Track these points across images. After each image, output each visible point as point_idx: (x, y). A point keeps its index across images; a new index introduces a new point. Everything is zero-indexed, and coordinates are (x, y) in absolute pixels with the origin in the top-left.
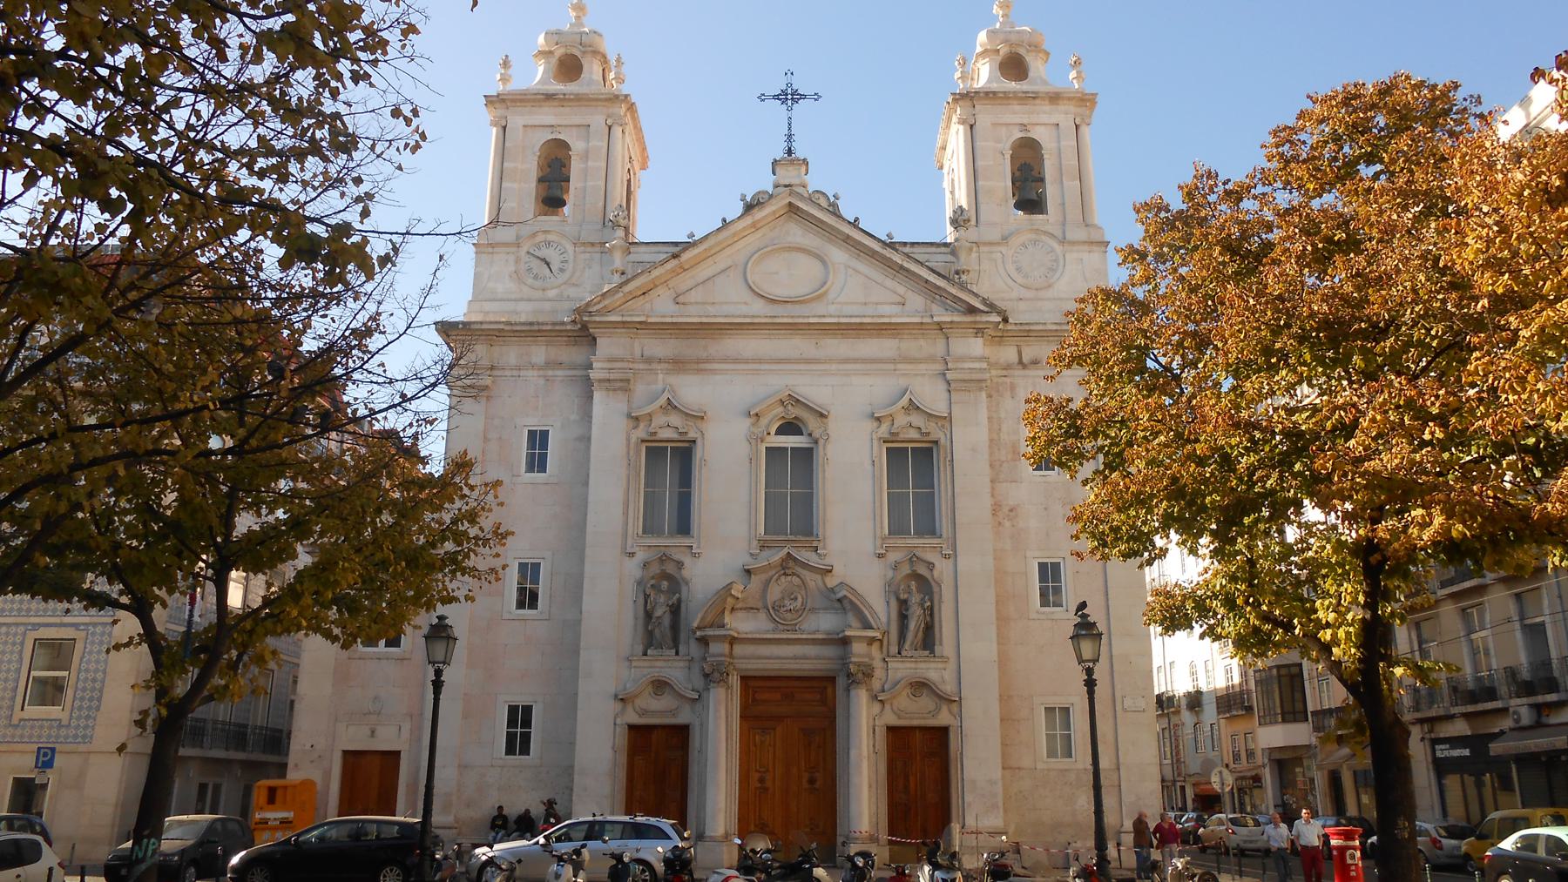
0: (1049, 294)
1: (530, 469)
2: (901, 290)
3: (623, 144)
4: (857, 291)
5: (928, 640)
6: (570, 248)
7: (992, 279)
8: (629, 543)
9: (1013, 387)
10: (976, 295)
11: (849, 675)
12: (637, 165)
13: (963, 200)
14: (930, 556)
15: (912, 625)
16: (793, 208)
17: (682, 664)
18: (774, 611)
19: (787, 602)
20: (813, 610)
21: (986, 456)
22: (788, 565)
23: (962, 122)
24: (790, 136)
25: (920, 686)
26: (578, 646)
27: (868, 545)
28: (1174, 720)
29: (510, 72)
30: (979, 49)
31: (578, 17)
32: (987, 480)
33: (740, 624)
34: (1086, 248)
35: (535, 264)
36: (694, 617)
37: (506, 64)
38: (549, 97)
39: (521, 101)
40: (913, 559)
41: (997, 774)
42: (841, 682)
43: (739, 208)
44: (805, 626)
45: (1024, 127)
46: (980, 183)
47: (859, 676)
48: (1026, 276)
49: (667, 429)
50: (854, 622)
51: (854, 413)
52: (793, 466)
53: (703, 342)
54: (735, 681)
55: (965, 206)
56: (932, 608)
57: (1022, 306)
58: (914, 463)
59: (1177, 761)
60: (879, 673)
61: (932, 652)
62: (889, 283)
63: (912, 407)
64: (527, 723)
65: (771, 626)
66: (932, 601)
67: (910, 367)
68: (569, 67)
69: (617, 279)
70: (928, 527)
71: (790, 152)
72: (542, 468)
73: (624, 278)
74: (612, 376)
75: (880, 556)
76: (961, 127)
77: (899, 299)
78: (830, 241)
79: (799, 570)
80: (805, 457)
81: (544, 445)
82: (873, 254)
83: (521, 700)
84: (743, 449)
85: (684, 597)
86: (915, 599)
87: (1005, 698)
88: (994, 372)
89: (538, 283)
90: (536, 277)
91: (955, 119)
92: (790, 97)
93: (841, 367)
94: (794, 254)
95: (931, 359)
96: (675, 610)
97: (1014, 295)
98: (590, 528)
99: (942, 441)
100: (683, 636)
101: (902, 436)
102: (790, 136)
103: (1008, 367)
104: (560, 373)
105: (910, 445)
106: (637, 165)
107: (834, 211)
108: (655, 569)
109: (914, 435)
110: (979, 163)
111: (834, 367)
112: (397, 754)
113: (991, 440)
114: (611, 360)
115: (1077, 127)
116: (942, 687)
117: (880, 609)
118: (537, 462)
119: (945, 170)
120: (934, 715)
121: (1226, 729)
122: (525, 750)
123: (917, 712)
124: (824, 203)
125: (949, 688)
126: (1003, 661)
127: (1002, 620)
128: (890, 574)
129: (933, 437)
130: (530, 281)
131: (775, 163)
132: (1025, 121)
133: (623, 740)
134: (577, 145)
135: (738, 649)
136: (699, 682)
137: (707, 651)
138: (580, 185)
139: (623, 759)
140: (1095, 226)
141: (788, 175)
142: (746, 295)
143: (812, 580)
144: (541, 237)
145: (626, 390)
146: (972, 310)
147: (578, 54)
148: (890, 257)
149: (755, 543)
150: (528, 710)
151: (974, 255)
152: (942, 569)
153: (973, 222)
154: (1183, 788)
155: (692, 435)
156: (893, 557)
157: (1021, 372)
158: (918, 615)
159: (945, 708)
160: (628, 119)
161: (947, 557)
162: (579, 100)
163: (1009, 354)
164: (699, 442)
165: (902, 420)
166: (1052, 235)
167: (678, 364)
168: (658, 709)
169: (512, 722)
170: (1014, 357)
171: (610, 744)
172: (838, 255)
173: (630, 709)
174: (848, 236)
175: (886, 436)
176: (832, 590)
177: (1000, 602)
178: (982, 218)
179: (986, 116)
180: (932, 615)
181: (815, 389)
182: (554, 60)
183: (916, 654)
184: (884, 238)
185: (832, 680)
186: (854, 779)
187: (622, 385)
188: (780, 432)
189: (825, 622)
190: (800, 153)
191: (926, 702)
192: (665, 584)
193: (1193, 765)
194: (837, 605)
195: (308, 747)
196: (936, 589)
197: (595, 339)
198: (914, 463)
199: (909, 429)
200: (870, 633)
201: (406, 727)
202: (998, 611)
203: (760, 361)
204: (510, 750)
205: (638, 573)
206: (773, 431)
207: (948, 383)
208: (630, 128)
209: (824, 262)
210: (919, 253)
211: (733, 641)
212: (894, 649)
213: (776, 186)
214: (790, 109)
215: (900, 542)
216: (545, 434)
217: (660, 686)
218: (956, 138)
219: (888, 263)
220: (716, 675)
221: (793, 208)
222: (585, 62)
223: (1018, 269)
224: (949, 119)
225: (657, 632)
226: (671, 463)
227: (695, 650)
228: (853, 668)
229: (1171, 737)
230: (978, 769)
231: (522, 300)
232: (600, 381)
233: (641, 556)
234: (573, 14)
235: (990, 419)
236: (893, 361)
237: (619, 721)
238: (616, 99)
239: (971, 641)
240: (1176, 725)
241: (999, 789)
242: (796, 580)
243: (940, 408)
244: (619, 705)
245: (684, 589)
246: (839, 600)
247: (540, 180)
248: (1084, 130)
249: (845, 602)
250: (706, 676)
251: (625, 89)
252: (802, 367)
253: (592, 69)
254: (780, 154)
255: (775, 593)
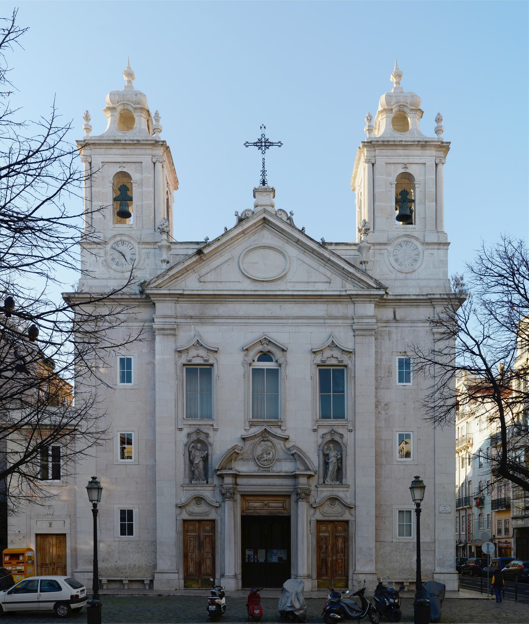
0: (414, 275)
1: (123, 381)
2: (329, 274)
3: (163, 174)
4: (304, 275)
5: (339, 474)
6: (136, 246)
7: (382, 268)
8: (180, 422)
9: (390, 333)
10: (371, 278)
11: (298, 494)
12: (171, 188)
13: (365, 216)
14: (341, 431)
15: (331, 468)
16: (265, 222)
17: (210, 488)
18: (257, 460)
19: (265, 455)
20: (279, 460)
21: (373, 374)
22: (265, 435)
23: (367, 161)
24: (264, 172)
25: (334, 500)
26: (155, 478)
27: (309, 425)
28: (469, 512)
29: (90, 123)
30: (380, 108)
31: (129, 82)
32: (374, 387)
33: (242, 467)
34: (436, 247)
35: (117, 255)
36: (215, 461)
37: (87, 118)
38: (116, 143)
39: (99, 144)
40: (333, 432)
41: (373, 544)
42: (293, 497)
43: (234, 221)
44: (274, 469)
45: (405, 166)
46: (376, 204)
47: (303, 495)
48: (400, 265)
49: (197, 357)
50: (302, 468)
51: (302, 343)
52: (266, 365)
53: (216, 306)
54: (238, 497)
55: (367, 220)
56: (341, 459)
57: (398, 283)
58: (332, 380)
59: (468, 532)
60: (313, 493)
61: (341, 482)
62: (322, 269)
63: (333, 346)
64: (131, 519)
65: (256, 468)
66: (341, 455)
67: (333, 321)
68: (126, 120)
69: (165, 266)
70: (340, 415)
71: (264, 183)
72: (129, 381)
73: (169, 266)
74: (166, 327)
75: (315, 430)
76: (366, 165)
77: (326, 280)
78: (288, 242)
79: (271, 438)
80: (274, 373)
81: (129, 367)
82: (313, 251)
83: (126, 507)
84: (240, 370)
85: (210, 453)
86: (333, 454)
87: (378, 506)
88: (379, 325)
89: (119, 268)
90: (117, 264)
91: (363, 159)
92: (263, 144)
93: (294, 321)
94: (267, 251)
95: (345, 318)
96: (205, 459)
97: (393, 276)
98: (157, 415)
99: (350, 366)
100: (210, 473)
101: (328, 363)
102: (264, 172)
103: (387, 322)
104: (135, 324)
105: (332, 368)
106: (171, 188)
107: (291, 225)
108: (194, 437)
109: (334, 362)
110: (376, 190)
111: (290, 321)
112: (65, 535)
113: (376, 365)
114: (164, 317)
115: (436, 164)
116: (346, 500)
117: (315, 460)
118: (126, 377)
119: (356, 192)
120: (342, 516)
121: (496, 518)
122: (131, 533)
123: (333, 512)
124: (285, 218)
125: (349, 501)
126: (378, 487)
127: (378, 465)
128: (320, 441)
129: (345, 363)
130: (114, 267)
131: (255, 191)
132: (406, 161)
133: (180, 528)
134: (135, 176)
135: (239, 481)
136: (219, 498)
137: (223, 482)
138: (139, 203)
139: (181, 538)
140: (443, 232)
141: (264, 199)
142: (240, 277)
143: (279, 444)
144: (118, 238)
145: (174, 335)
146: (369, 287)
147: (131, 109)
148: (321, 252)
149: (247, 423)
150: (130, 512)
151: (371, 251)
152: (348, 438)
153: (372, 230)
154: (470, 547)
155: (211, 362)
156: (322, 431)
157: (394, 325)
158: (334, 463)
159: (347, 511)
160: (165, 158)
161: (350, 431)
162: (137, 143)
163: (388, 313)
164: (215, 366)
165: (328, 353)
166: (417, 239)
167: (202, 319)
168: (198, 511)
169: (122, 519)
170: (391, 316)
171: (175, 530)
172: (292, 251)
173: (184, 512)
174: (298, 240)
175: (319, 363)
176: (289, 449)
177: (377, 455)
178: (377, 227)
179: (383, 156)
180: (341, 463)
181: (279, 335)
182: (117, 114)
183: (333, 483)
184: (320, 241)
185: (289, 496)
186: (300, 553)
187: (172, 332)
188: (259, 360)
189: (287, 467)
190: (270, 184)
191: (338, 508)
192: (199, 445)
193: (476, 534)
194: (292, 457)
195: (17, 532)
196: (344, 448)
197: (154, 304)
198: (332, 380)
199: (332, 358)
200: (309, 473)
201: (68, 521)
202: (376, 460)
203: (248, 318)
204: (123, 533)
205: (185, 440)
206: (256, 360)
207: (354, 331)
208: (166, 164)
209: (284, 256)
210: (341, 251)
211: (236, 476)
212: (321, 481)
213: (256, 206)
214: (263, 153)
215: (326, 422)
216: (129, 360)
217: (199, 499)
218: (362, 172)
219: (321, 257)
220: (228, 494)
221: (265, 222)
222: (135, 115)
223: (396, 260)
224: (359, 159)
225: (196, 472)
226: (199, 374)
227: (216, 481)
228: (299, 491)
229: (464, 523)
230: (363, 539)
231: (110, 278)
232: (159, 329)
233: (186, 431)
234: (126, 79)
235: (376, 352)
236: (324, 318)
237: (178, 518)
238: (156, 143)
239: (361, 476)
240: (469, 515)
241: (373, 552)
242: (269, 444)
243: (349, 346)
244: (179, 510)
245: (210, 448)
246: (293, 455)
247: (115, 200)
248: (440, 166)
249: (296, 456)
250: (223, 495)
251: (162, 136)
252: (272, 321)
253: (140, 122)
254: (257, 184)
255: (259, 450)
